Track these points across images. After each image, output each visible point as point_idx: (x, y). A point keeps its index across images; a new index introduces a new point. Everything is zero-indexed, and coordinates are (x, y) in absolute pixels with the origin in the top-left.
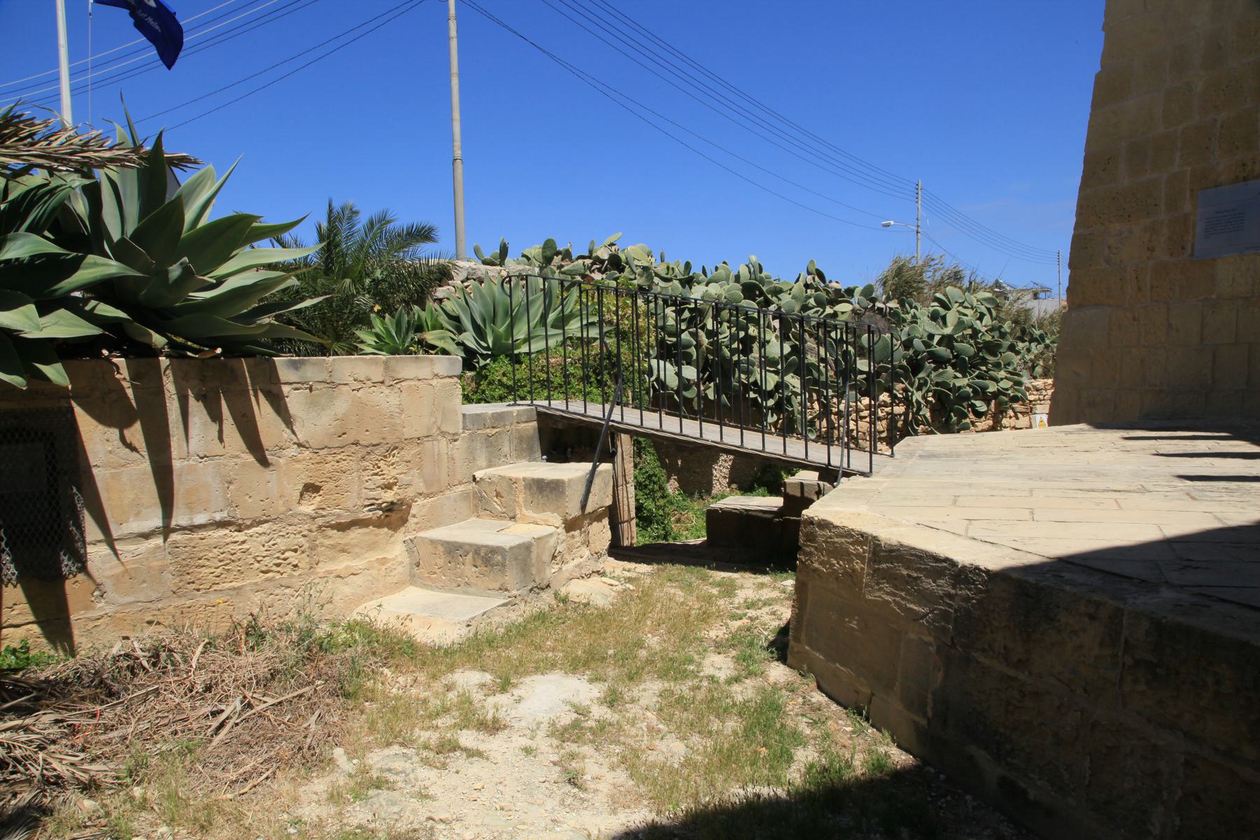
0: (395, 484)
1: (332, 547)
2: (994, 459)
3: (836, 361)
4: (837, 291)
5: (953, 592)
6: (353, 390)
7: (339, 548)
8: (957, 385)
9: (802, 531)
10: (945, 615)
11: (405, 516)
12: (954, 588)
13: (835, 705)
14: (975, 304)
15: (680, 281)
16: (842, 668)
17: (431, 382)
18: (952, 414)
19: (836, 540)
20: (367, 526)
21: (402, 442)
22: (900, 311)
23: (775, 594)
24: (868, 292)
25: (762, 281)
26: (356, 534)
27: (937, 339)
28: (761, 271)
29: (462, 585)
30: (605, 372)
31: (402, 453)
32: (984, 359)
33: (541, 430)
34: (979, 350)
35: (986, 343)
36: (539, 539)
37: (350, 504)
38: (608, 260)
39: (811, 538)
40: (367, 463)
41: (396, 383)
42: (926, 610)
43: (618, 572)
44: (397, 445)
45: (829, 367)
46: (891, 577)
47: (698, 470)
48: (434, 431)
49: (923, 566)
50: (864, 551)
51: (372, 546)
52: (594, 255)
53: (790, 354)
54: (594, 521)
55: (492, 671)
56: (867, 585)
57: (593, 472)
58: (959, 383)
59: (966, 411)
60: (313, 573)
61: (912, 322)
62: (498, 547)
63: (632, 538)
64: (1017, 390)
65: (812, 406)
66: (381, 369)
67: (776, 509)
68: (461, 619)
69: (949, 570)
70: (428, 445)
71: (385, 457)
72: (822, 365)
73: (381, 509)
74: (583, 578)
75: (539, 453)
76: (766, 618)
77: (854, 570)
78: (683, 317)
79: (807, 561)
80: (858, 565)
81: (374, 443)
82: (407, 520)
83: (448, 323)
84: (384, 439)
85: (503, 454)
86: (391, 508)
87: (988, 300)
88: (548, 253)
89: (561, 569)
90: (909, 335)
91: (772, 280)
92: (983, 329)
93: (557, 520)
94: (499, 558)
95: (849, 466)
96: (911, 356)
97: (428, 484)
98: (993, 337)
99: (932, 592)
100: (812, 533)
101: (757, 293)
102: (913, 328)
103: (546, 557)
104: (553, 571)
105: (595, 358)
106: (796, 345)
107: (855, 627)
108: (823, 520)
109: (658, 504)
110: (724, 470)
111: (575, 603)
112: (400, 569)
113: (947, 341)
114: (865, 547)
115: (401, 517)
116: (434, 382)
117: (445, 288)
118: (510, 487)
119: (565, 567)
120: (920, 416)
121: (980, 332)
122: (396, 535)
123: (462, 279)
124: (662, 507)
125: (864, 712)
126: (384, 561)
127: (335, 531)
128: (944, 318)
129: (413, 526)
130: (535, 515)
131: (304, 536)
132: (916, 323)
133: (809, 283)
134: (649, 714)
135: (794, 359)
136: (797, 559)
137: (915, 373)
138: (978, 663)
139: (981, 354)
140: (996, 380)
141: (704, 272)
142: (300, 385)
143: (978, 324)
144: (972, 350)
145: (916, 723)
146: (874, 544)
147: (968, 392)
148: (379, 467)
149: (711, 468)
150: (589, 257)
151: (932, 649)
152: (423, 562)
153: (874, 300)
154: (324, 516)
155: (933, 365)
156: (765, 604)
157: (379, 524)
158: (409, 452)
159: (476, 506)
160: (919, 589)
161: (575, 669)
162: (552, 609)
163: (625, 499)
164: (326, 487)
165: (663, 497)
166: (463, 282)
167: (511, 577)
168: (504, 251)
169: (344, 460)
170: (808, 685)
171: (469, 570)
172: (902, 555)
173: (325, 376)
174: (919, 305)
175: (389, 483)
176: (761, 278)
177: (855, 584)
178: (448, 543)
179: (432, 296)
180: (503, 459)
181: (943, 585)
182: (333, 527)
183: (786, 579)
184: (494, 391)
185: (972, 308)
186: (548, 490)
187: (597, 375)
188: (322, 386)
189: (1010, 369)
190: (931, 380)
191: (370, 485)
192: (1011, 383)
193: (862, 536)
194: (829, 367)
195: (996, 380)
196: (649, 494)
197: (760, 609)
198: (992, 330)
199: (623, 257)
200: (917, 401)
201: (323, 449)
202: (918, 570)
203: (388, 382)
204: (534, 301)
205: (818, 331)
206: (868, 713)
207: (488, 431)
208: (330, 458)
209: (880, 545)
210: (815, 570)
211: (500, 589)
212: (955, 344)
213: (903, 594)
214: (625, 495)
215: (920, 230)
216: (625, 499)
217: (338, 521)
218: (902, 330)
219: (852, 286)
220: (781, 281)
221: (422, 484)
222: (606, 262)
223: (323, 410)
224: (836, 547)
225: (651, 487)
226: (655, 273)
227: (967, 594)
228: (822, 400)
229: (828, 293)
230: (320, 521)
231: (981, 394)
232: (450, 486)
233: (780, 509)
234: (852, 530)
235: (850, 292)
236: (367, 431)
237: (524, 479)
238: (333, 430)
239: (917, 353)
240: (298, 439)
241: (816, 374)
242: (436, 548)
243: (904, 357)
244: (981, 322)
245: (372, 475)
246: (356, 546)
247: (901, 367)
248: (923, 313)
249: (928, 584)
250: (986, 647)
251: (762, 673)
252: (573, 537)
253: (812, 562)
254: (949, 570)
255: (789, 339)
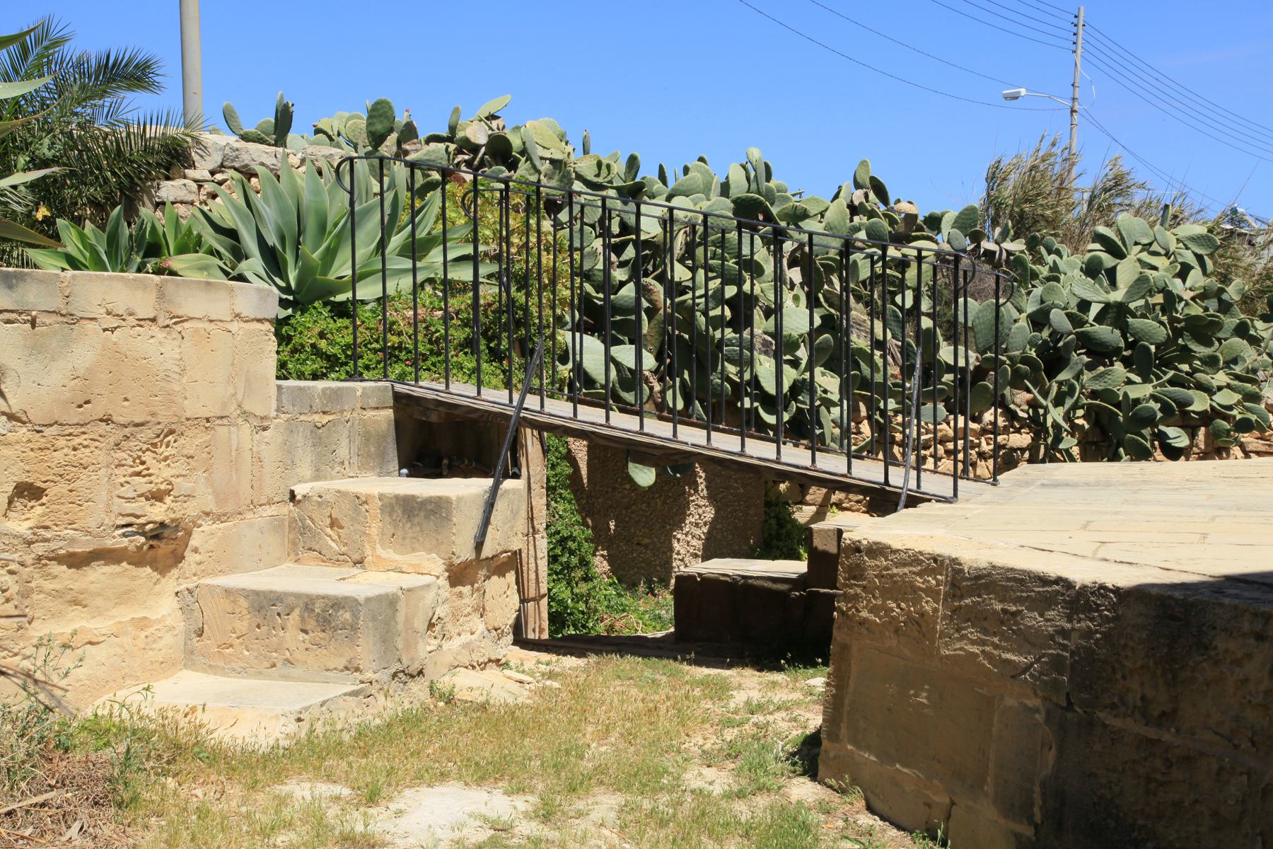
0: (168, 492)
1: (57, 594)
2: (1168, 490)
3: (905, 351)
4: (910, 218)
5: (1068, 626)
6: (105, 330)
7: (68, 597)
8: (1132, 396)
9: (843, 563)
10: (1057, 663)
11: (179, 550)
12: (1070, 620)
13: (895, 831)
14: (1172, 249)
15: (618, 189)
16: (905, 770)
17: (229, 326)
18: (1121, 450)
19: (895, 571)
20: (118, 562)
21: (182, 423)
22: (1028, 258)
23: (797, 696)
24: (966, 222)
25: (770, 196)
26: (98, 574)
27: (1095, 309)
28: (768, 178)
29: (279, 665)
30: (504, 335)
31: (182, 441)
32: (1185, 349)
33: (398, 424)
34: (1178, 333)
35: (1191, 319)
36: (409, 590)
37: (92, 523)
38: (487, 145)
39: (857, 573)
40: (124, 455)
41: (176, 323)
42: (1031, 658)
43: (529, 665)
44: (173, 427)
45: (889, 358)
46: (979, 618)
47: (646, 541)
48: (232, 410)
49: (1025, 595)
50: (938, 584)
51: (125, 597)
52: (460, 135)
53: (820, 331)
54: (494, 574)
55: (347, 780)
56: (942, 635)
57: (495, 490)
58: (1135, 392)
59: (1148, 445)
60: (22, 636)
61: (1048, 279)
62: (346, 598)
63: (541, 631)
64: (1249, 409)
65: (858, 428)
66: (152, 297)
67: (794, 576)
68: (287, 709)
69: (1063, 595)
70: (222, 431)
71: (154, 445)
72: (878, 353)
73: (143, 534)
74: (474, 667)
75: (395, 464)
76: (783, 726)
77: (922, 615)
78: (624, 257)
79: (850, 609)
80: (928, 606)
81: (137, 420)
82: (184, 558)
83: (217, 240)
84: (153, 415)
85: (338, 460)
86: (158, 533)
87: (1196, 239)
88: (379, 127)
89: (440, 646)
90: (1042, 302)
91: (788, 194)
92: (1187, 295)
93: (436, 566)
94: (347, 616)
95: (919, 486)
96: (1045, 342)
97: (220, 498)
98: (1206, 309)
99: (1038, 630)
100: (858, 566)
101: (761, 217)
102: (1051, 289)
103: (421, 625)
104: (429, 648)
105: (485, 311)
106: (831, 315)
107: (925, 701)
108: (876, 543)
109: (576, 590)
110: (694, 542)
111: (466, 702)
112: (169, 639)
113: (1116, 314)
114: (939, 577)
115: (173, 552)
116: (234, 327)
117: (178, 182)
118: (356, 510)
119: (446, 645)
120: (1060, 451)
121: (1181, 299)
122: (163, 581)
123: (211, 167)
124: (586, 598)
125: (939, 833)
126: (142, 623)
127: (65, 567)
128: (1111, 274)
129: (194, 568)
130: (397, 557)
131: (11, 572)
132: (1057, 280)
133: (856, 203)
134: (605, 832)
135: (826, 340)
136: (834, 609)
137: (1051, 374)
138: (1105, 726)
139: (1180, 341)
140: (1209, 391)
141: (662, 177)
142: (14, 316)
143: (1177, 286)
144: (1162, 333)
145: (1017, 836)
146: (953, 569)
147: (1153, 409)
148: (143, 463)
149: (669, 537)
150: (450, 139)
151: (1039, 717)
152: (210, 627)
153: (976, 237)
154: (47, 540)
155: (1086, 359)
156: (779, 709)
157: (138, 560)
158: (192, 442)
159: (294, 544)
160: (1019, 629)
161: (482, 778)
162: (426, 709)
163: (532, 560)
164: (53, 491)
165: (586, 579)
166: (213, 173)
167: (366, 649)
168: (283, 121)
169: (85, 447)
170: (852, 804)
171: (292, 637)
172: (994, 583)
173: (57, 303)
174: (1065, 250)
175: (159, 490)
176: (769, 190)
177: (924, 636)
178: (257, 593)
179: (151, 197)
180: (338, 469)
181: (1056, 618)
182: (60, 560)
183: (813, 676)
184: (304, 362)
185: (1167, 255)
186: (422, 514)
187: (490, 340)
188: (54, 318)
189: (1238, 369)
190: (1083, 387)
191: (128, 491)
192: (1238, 397)
193: (935, 561)
194: (889, 358)
195: (1209, 391)
196: (561, 572)
197: (771, 713)
198: (1204, 295)
199: (516, 142)
200: (1056, 425)
201: (51, 425)
202: (1019, 600)
203: (162, 321)
204: (367, 212)
205: (872, 291)
206: (945, 833)
207: (317, 417)
208: (62, 442)
209: (962, 571)
210: (864, 622)
211: (347, 668)
212: (1130, 320)
213: (996, 640)
214: (532, 552)
215: (1077, 107)
216: (532, 560)
217: (71, 550)
218: (1029, 293)
219: (938, 212)
220: (805, 197)
221: (210, 497)
222: (483, 150)
223: (53, 359)
224: (896, 582)
225: (564, 559)
226: (576, 173)
227: (1089, 627)
228: (877, 417)
229: (892, 222)
230: (39, 549)
231: (1178, 413)
232: (254, 505)
233: (802, 576)
234: (921, 553)
235: (934, 222)
236: (126, 399)
237: (381, 497)
238: (68, 395)
239: (1056, 335)
240: (9, 406)
241: (866, 370)
242: (234, 602)
243: (1032, 343)
244: (1184, 281)
245: (131, 476)
246: (99, 594)
247: (1026, 360)
248: (1071, 263)
249: (1033, 619)
250: (1116, 700)
251: (779, 788)
252: (460, 595)
253: (858, 611)
254: (1063, 595)
255: (819, 305)
